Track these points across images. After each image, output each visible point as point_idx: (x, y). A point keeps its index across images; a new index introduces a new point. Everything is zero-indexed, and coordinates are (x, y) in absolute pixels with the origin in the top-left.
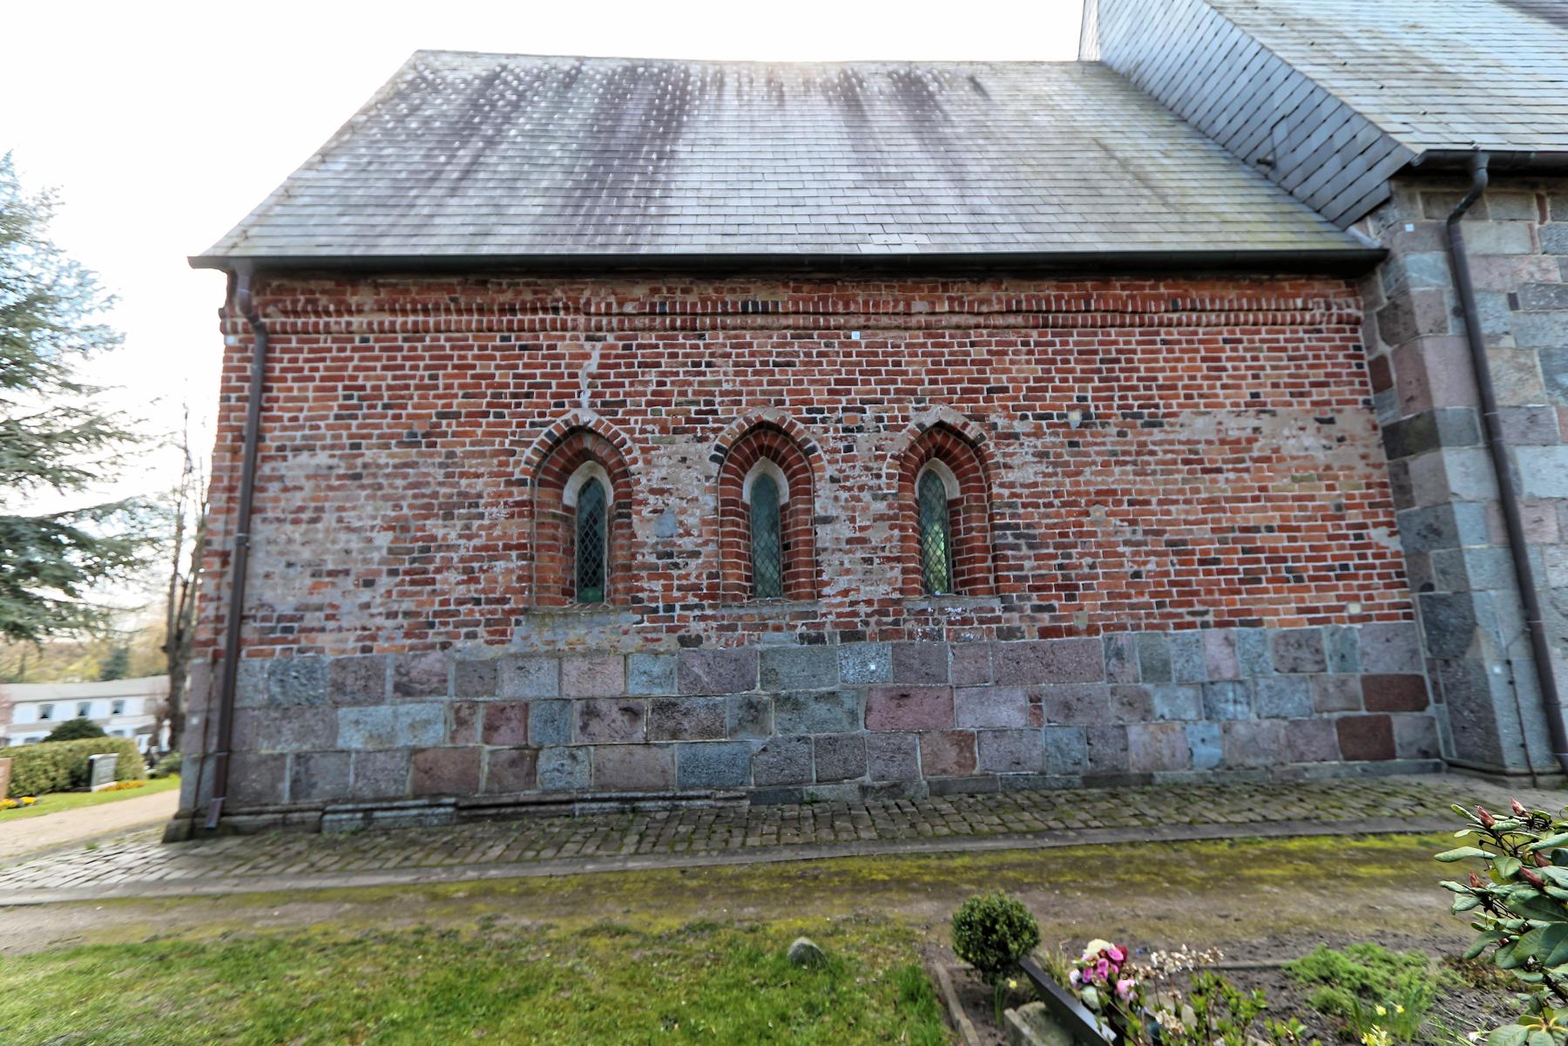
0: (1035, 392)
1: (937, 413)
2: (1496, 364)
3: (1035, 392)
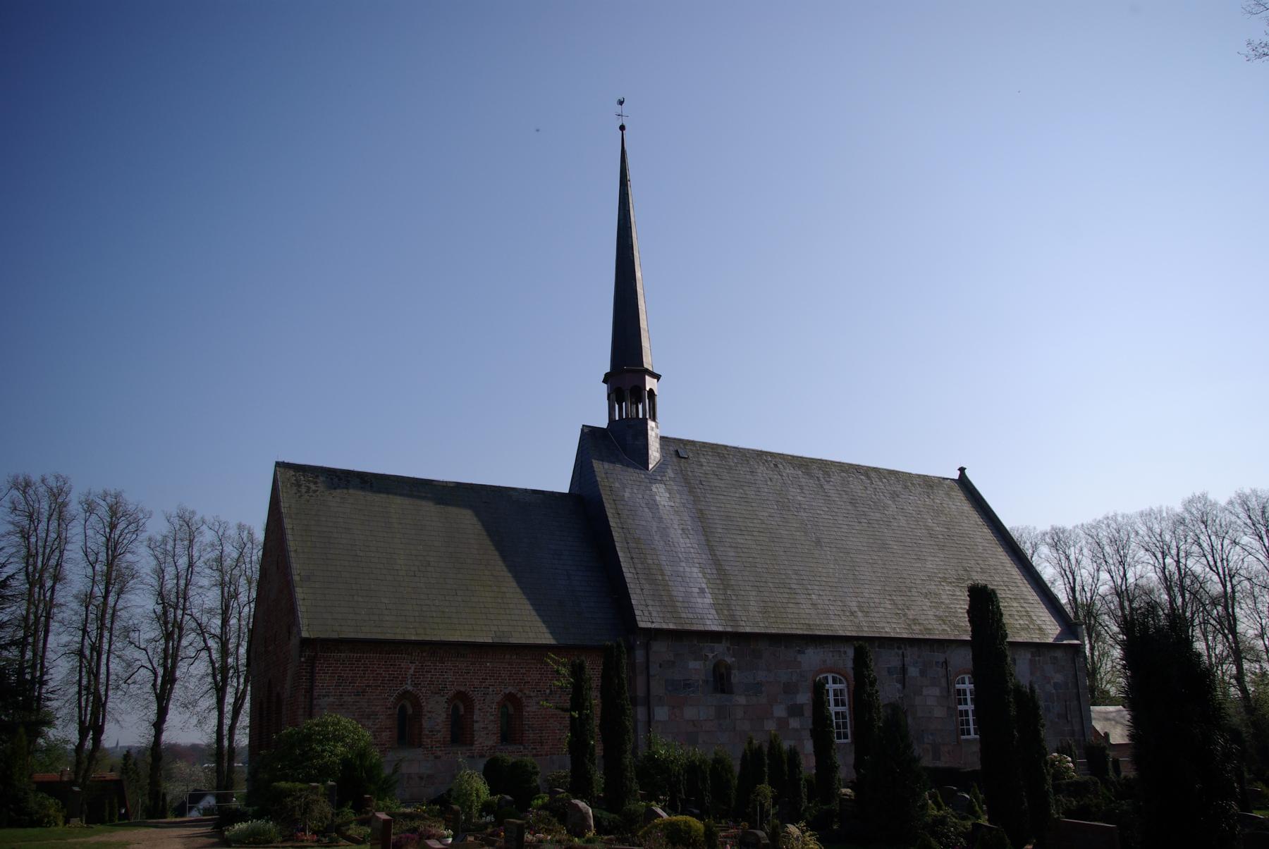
1: (510, 689)
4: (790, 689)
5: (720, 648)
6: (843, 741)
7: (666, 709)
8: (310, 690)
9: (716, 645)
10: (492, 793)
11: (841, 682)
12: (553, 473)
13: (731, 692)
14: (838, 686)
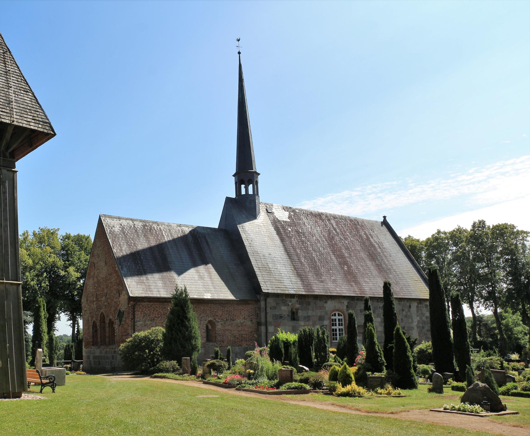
0: (221, 316)
1: (210, 319)
2: (268, 316)
3: (221, 316)
4: (321, 318)
5: (294, 300)
6: (335, 341)
7: (273, 327)
8: (134, 318)
9: (293, 299)
10: (245, 360)
11: (341, 316)
12: (212, 219)
13: (298, 320)
14: (340, 317)
